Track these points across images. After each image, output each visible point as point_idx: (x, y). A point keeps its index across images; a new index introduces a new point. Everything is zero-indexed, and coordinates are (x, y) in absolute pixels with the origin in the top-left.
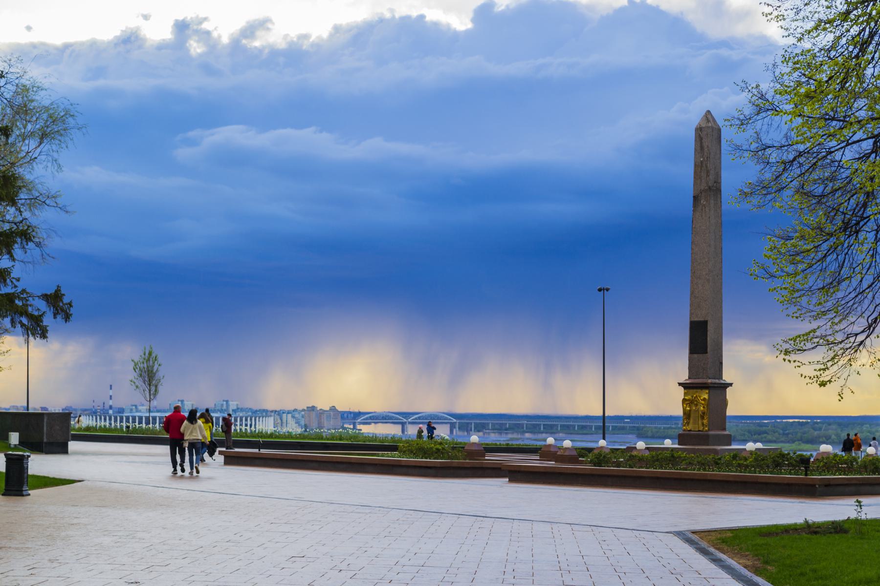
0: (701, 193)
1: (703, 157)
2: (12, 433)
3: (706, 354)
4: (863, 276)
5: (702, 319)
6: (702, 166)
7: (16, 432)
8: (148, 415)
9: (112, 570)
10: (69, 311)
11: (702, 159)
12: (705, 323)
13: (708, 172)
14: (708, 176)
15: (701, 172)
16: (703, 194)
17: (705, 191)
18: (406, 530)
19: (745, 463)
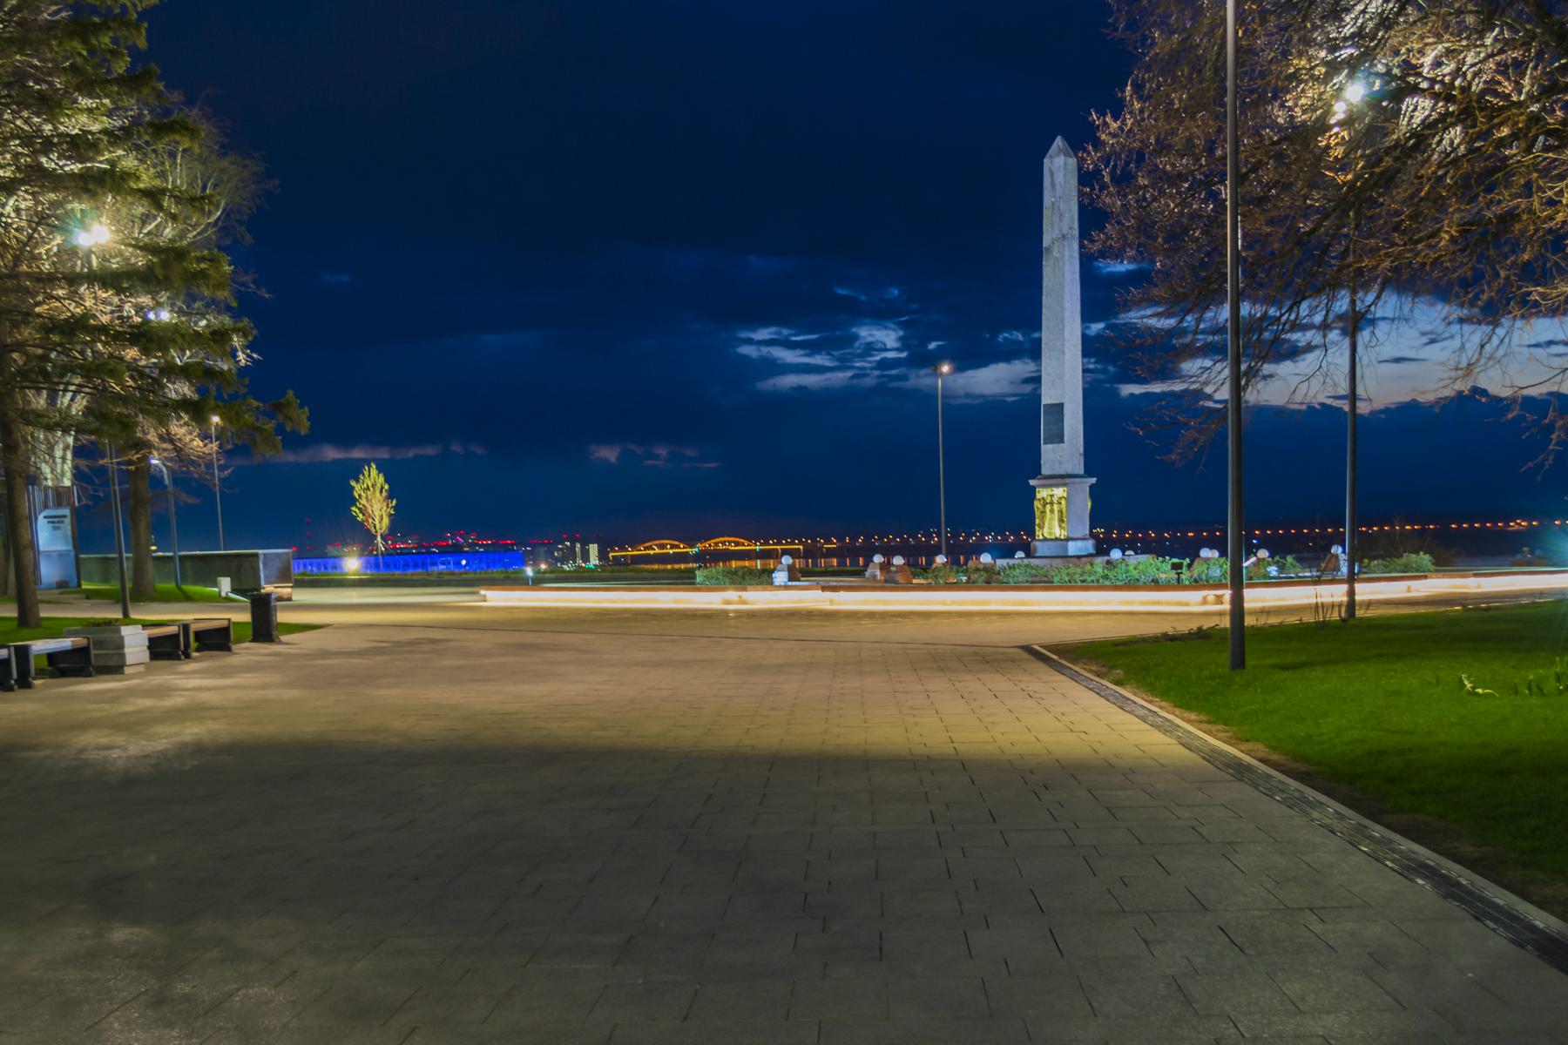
0: (1053, 242)
1: (1054, 196)
2: (221, 578)
3: (1063, 445)
4: (1452, 386)
5: (1057, 402)
6: (1053, 209)
7: (1231, 624)
8: (1358, 587)
9: (830, 883)
10: (1247, 384)
11: (1053, 200)
12: (1061, 405)
13: (1061, 215)
14: (1061, 220)
15: (1052, 216)
16: (1056, 244)
17: (1058, 239)
18: (906, 727)
19: (583, 565)
